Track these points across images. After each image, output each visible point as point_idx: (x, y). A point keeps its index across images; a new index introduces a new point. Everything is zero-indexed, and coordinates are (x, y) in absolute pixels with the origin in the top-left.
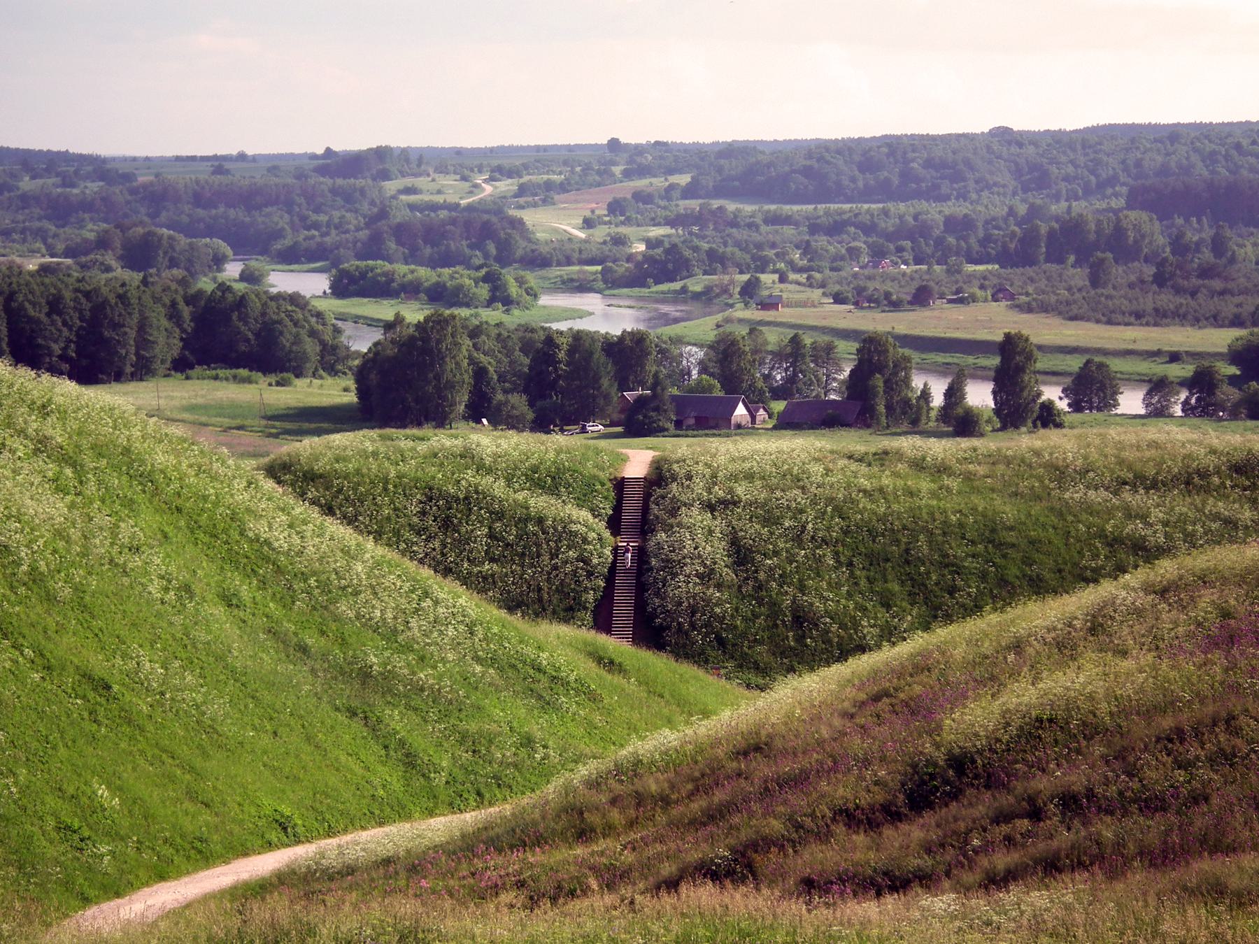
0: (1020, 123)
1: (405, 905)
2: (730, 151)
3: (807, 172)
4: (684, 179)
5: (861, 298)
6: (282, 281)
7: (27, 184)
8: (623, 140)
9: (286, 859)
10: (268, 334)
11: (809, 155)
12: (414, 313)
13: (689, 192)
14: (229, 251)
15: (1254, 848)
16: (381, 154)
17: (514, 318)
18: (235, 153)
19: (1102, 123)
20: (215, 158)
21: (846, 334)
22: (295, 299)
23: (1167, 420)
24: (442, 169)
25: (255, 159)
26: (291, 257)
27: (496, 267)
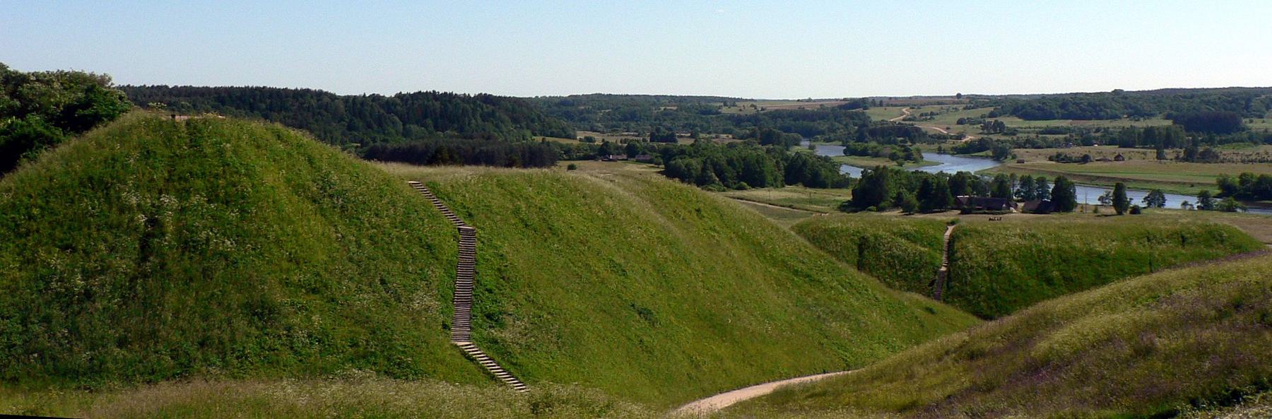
0: (1127, 88)
1: (187, 397)
3: (1039, 109)
5: (1058, 158)
7: (725, 110)
8: (962, 94)
9: (772, 390)
10: (816, 175)
11: (1039, 101)
13: (992, 115)
14: (801, 137)
15: (1260, 387)
16: (864, 100)
17: (910, 167)
18: (807, 98)
19: (1183, 87)
20: (752, 100)
21: (1052, 173)
22: (827, 159)
23: (1234, 213)
24: (904, 106)
25: (815, 101)
27: (269, 112)
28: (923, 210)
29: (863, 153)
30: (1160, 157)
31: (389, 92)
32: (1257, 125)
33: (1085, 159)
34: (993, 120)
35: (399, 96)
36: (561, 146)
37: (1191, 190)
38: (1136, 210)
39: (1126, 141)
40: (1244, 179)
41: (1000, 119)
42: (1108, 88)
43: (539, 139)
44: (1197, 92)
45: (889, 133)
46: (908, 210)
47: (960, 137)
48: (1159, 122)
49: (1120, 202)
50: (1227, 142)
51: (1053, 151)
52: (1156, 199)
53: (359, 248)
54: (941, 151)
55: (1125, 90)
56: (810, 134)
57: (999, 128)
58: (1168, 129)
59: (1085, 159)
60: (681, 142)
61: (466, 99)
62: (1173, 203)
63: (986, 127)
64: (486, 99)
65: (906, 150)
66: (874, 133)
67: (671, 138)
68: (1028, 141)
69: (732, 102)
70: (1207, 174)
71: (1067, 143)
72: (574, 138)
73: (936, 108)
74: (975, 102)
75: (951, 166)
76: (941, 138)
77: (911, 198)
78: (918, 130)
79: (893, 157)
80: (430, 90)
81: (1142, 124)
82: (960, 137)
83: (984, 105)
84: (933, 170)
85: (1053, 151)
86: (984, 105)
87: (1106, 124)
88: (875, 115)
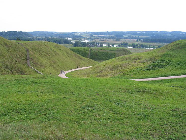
2: (93, 32)
4: (90, 34)
6: (69, 39)
7: (55, 33)
12: (76, 41)
13: (91, 34)
26: (69, 38)
28: (83, 47)
29: (74, 39)
30: (113, 40)
31: (6, 31)
32: (125, 36)
33: (104, 40)
34: (91, 35)
35: (8, 32)
36: (33, 39)
37: (117, 44)
38: (111, 47)
39: (108, 38)
40: (124, 43)
41: (92, 35)
42: (106, 31)
43: (29, 38)
44: (33, 33)
45: (78, 37)
46: (81, 46)
47: (87, 37)
48: (113, 36)
49: (109, 46)
50: (121, 38)
51: (99, 39)
52: (113, 45)
53: (124, 74)
54: (85, 39)
55: (106, 31)
56: (67, 37)
57: (92, 36)
58: (114, 37)
59: (104, 40)
60: (49, 38)
61: (18, 32)
62: (115, 46)
63: (90, 36)
64: (21, 32)
65: (80, 39)
66: (76, 36)
67: (48, 37)
68: (96, 38)
69: (56, 32)
70: (119, 42)
71: (100, 38)
72: (34, 37)
73: (84, 33)
74: (89, 33)
75: (87, 41)
76: (84, 37)
77: (81, 45)
78: (81, 36)
79: (78, 40)
80: (13, 31)
81: (110, 36)
82: (87, 37)
83: (90, 33)
84: (84, 42)
85: (99, 39)
86: (90, 33)
87: (106, 36)
88: (76, 34)
